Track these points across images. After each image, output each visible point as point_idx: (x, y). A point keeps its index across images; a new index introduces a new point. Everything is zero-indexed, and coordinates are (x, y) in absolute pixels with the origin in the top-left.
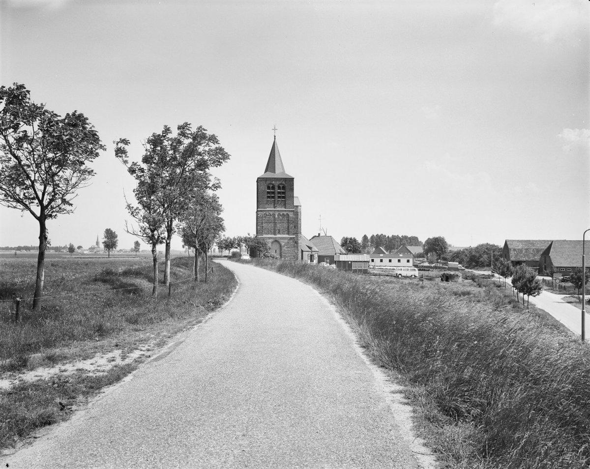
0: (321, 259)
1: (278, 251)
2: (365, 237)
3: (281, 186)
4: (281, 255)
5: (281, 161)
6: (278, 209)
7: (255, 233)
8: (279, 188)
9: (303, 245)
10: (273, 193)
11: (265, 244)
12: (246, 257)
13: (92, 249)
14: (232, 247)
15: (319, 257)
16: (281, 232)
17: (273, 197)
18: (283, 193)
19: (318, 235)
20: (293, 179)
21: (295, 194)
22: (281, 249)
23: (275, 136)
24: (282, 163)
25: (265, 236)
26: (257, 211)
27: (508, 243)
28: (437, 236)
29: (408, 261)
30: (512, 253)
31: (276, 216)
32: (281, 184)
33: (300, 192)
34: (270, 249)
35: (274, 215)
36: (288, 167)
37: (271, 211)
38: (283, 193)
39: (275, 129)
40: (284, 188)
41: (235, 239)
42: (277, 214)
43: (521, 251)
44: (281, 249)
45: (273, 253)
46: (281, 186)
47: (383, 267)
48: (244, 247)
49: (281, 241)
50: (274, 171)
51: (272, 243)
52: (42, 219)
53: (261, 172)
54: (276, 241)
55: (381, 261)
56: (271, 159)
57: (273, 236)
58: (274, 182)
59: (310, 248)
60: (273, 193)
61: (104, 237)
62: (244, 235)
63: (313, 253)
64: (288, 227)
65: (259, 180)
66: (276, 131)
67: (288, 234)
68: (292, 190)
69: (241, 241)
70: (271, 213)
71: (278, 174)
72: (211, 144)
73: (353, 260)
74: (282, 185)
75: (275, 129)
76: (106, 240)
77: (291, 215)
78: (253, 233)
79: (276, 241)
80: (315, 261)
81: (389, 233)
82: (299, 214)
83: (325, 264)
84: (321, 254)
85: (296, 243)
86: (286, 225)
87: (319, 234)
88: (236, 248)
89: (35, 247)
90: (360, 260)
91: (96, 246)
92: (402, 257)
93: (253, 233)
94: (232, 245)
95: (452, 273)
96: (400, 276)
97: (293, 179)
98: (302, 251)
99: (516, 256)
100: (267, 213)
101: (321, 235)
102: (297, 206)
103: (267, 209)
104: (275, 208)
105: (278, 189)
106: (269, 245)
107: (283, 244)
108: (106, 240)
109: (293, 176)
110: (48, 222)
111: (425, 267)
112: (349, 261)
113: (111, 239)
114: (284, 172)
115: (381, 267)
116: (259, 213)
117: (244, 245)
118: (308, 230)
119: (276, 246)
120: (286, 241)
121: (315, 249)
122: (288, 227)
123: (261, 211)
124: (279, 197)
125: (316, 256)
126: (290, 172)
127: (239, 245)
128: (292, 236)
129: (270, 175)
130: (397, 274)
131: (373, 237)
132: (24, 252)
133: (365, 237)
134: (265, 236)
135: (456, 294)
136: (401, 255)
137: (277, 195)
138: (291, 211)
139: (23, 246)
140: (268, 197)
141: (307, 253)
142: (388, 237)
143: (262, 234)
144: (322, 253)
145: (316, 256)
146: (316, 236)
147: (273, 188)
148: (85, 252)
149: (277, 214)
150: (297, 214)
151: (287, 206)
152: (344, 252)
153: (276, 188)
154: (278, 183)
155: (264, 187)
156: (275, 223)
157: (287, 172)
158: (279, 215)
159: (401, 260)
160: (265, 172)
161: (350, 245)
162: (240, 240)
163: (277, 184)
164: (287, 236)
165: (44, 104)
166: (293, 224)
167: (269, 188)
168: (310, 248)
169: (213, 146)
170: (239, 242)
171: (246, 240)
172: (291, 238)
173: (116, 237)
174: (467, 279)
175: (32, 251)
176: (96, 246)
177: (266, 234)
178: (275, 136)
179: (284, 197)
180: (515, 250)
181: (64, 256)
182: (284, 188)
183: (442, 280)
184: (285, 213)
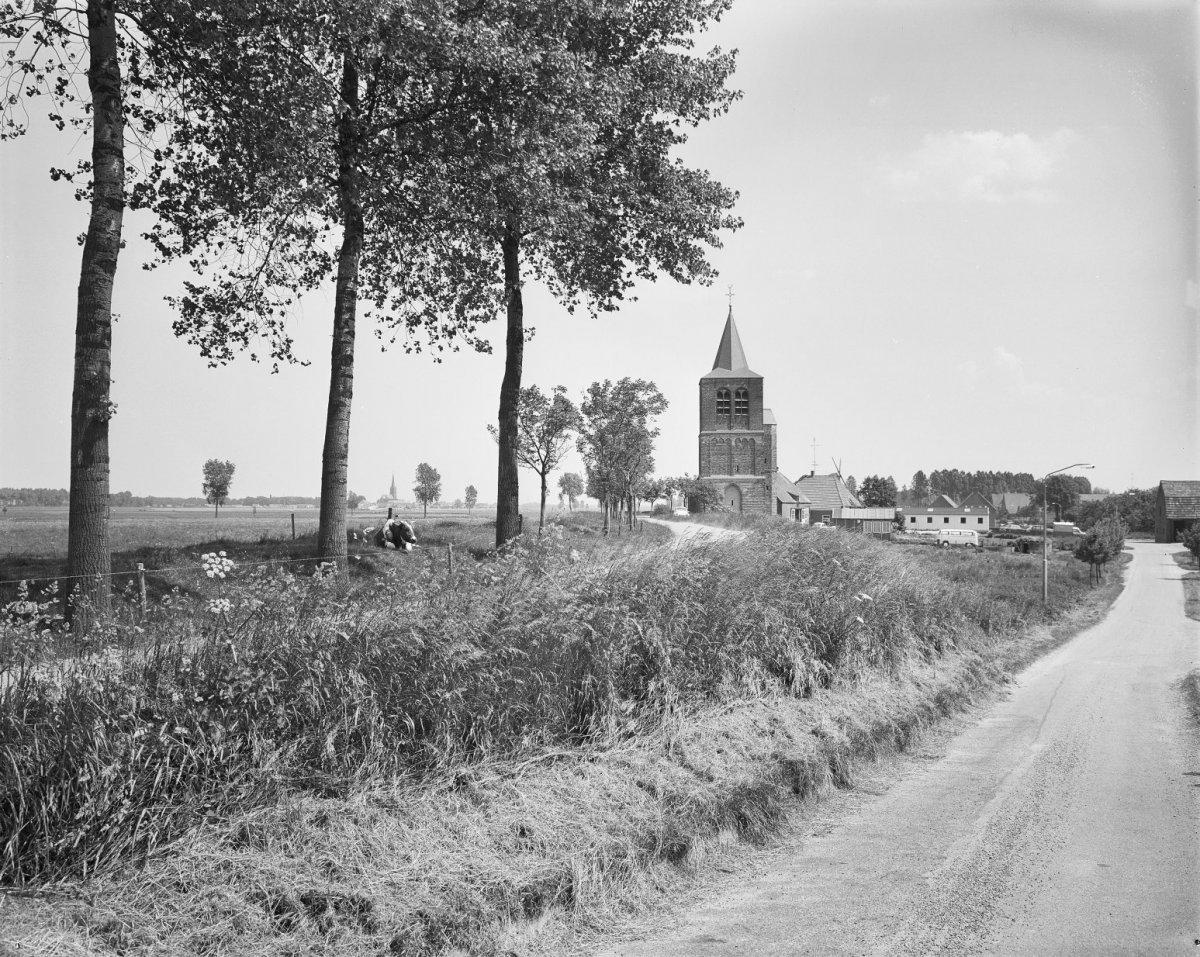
0: (815, 516)
1: (736, 503)
2: (920, 476)
3: (741, 392)
5: (741, 348)
6: (736, 431)
7: (697, 474)
8: (738, 395)
9: (780, 491)
10: (728, 403)
12: (684, 512)
13: (383, 501)
14: (656, 496)
15: (812, 513)
17: (728, 411)
18: (745, 403)
19: (809, 474)
20: (760, 380)
21: (766, 405)
24: (743, 352)
25: (713, 477)
26: (700, 436)
27: (1164, 487)
28: (1029, 473)
29: (980, 521)
30: (1171, 506)
31: (733, 444)
32: (741, 388)
33: (773, 402)
34: (722, 498)
36: (754, 359)
38: (745, 403)
39: (730, 295)
41: (661, 482)
42: (733, 440)
43: (1187, 501)
45: (728, 506)
46: (741, 392)
47: (931, 532)
48: (677, 496)
50: (728, 366)
51: (726, 488)
52: (543, 474)
53: (706, 369)
54: (733, 485)
55: (930, 520)
56: (722, 356)
57: (727, 477)
59: (795, 497)
60: (728, 403)
61: (415, 479)
62: (676, 474)
63: (801, 506)
65: (703, 383)
68: (760, 397)
69: (673, 486)
71: (736, 372)
72: (649, 392)
73: (865, 517)
75: (730, 295)
76: (419, 484)
77: (759, 441)
78: (692, 471)
79: (733, 485)
80: (805, 520)
81: (970, 466)
83: (820, 525)
84: (813, 508)
85: (769, 488)
86: (749, 459)
87: (812, 472)
88: (664, 497)
89: (278, 498)
90: (878, 517)
91: (391, 497)
92: (967, 514)
93: (692, 471)
94: (657, 493)
95: (1035, 538)
96: (946, 544)
97: (760, 380)
98: (780, 503)
99: (1178, 511)
101: (816, 474)
102: (769, 426)
103: (719, 431)
105: (737, 397)
106: (722, 492)
107: (745, 491)
108: (419, 484)
109: (761, 374)
110: (547, 477)
111: (1013, 531)
112: (856, 520)
113: (428, 483)
114: (746, 368)
115: (928, 532)
117: (678, 492)
118: (790, 464)
120: (750, 485)
121: (804, 498)
124: (738, 411)
125: (806, 511)
126: (756, 368)
127: (669, 493)
128: (760, 477)
129: (722, 373)
130: (938, 540)
131: (935, 475)
132: (274, 508)
133: (920, 476)
134: (713, 477)
135: (877, 536)
136: (967, 510)
137: (734, 408)
138: (757, 434)
139: (255, 497)
140: (719, 411)
141: (789, 506)
142: (969, 474)
143: (709, 474)
144: (818, 506)
145: (806, 511)
147: (728, 395)
148: (371, 508)
149: (733, 440)
150: (768, 438)
152: (859, 505)
153: (733, 395)
155: (711, 394)
159: (968, 518)
161: (878, 492)
162: (671, 484)
163: (733, 388)
164: (752, 477)
166: (762, 456)
167: (720, 395)
168: (795, 497)
169: (652, 394)
170: (668, 487)
171: (682, 484)
172: (758, 481)
173: (439, 478)
174: (1063, 549)
175: (271, 506)
176: (391, 497)
177: (716, 473)
179: (745, 411)
180: (1176, 499)
182: (746, 395)
183: (1016, 550)
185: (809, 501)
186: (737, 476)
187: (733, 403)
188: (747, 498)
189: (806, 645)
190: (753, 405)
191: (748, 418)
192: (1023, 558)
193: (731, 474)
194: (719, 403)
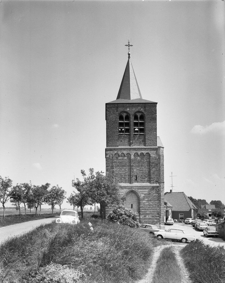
1: (135, 206)
3: (139, 115)
4: (139, 212)
10: (128, 124)
11: (115, 189)
15: (173, 212)
16: (139, 179)
17: (127, 131)
19: (170, 192)
20: (154, 105)
22: (139, 203)
23: (129, 54)
31: (132, 157)
32: (139, 112)
35: (129, 154)
37: (124, 149)
40: (142, 117)
42: (133, 153)
44: (139, 203)
46: (139, 115)
49: (139, 191)
50: (129, 97)
51: (127, 194)
54: (132, 192)
58: (128, 109)
64: (149, 172)
66: (127, 44)
67: (149, 181)
70: (125, 152)
71: (134, 96)
74: (140, 114)
77: (153, 154)
79: (132, 192)
82: (161, 158)
84: (174, 209)
86: (145, 170)
87: (171, 191)
96: (160, 237)
97: (154, 105)
100: (120, 153)
101: (173, 191)
103: (120, 147)
104: (130, 146)
107: (142, 196)
116: (108, 152)
119: (131, 200)
122: (149, 172)
123: (111, 150)
128: (155, 185)
137: (132, 127)
146: (167, 193)
147: (128, 118)
149: (133, 153)
151: (148, 142)
153: (132, 118)
154: (134, 110)
155: (115, 116)
156: (130, 166)
157: (143, 98)
158: (136, 155)
160: (117, 99)
164: (148, 184)
165: (76, 181)
167: (121, 118)
172: (153, 188)
178: (129, 54)
181: (13, 212)
184: (144, 152)
185: (172, 206)
186: (135, 184)
187: (132, 124)
188: (144, 202)
189: (64, 248)
190: (148, 126)
191: (144, 136)
192: (177, 233)
193: (130, 183)
194: (121, 124)
